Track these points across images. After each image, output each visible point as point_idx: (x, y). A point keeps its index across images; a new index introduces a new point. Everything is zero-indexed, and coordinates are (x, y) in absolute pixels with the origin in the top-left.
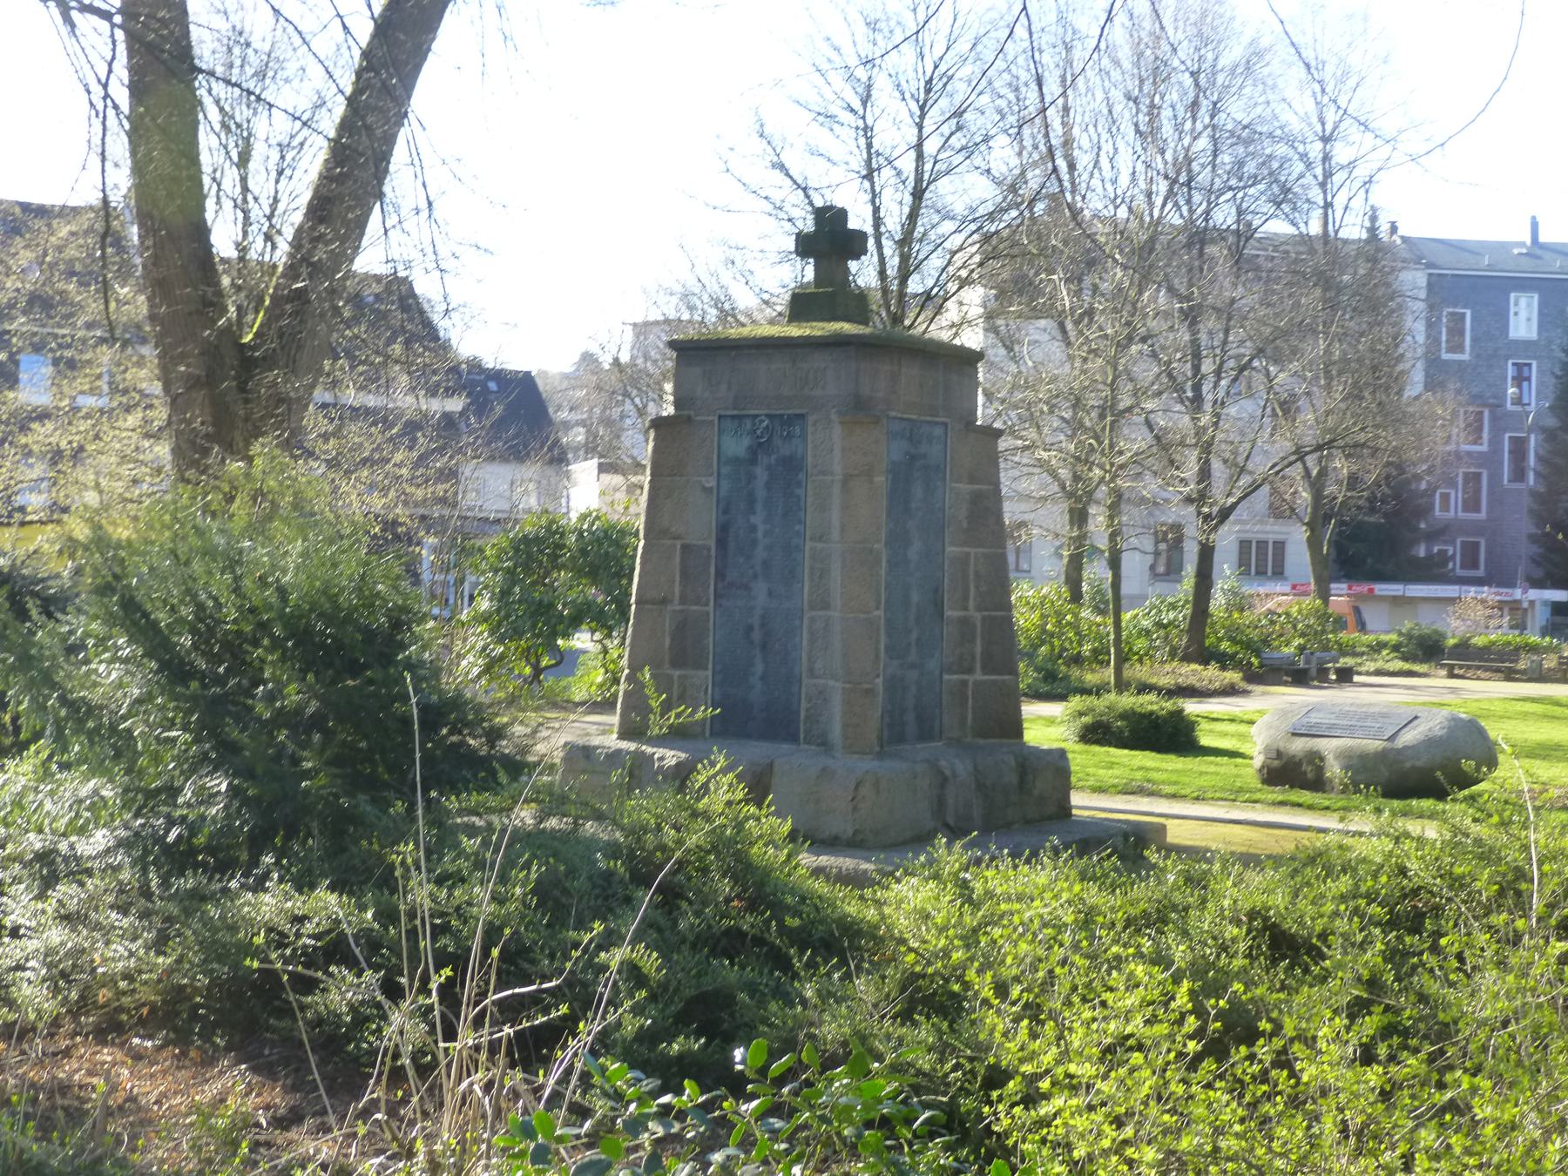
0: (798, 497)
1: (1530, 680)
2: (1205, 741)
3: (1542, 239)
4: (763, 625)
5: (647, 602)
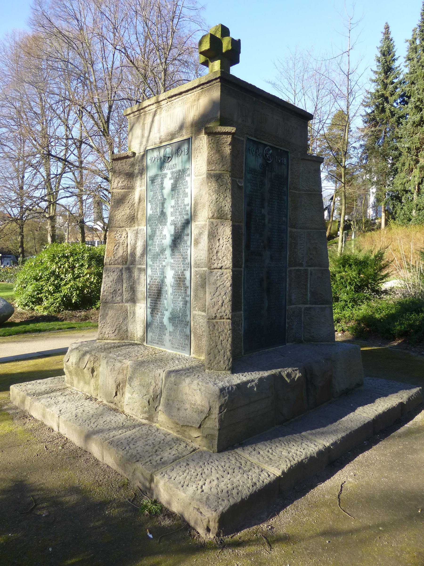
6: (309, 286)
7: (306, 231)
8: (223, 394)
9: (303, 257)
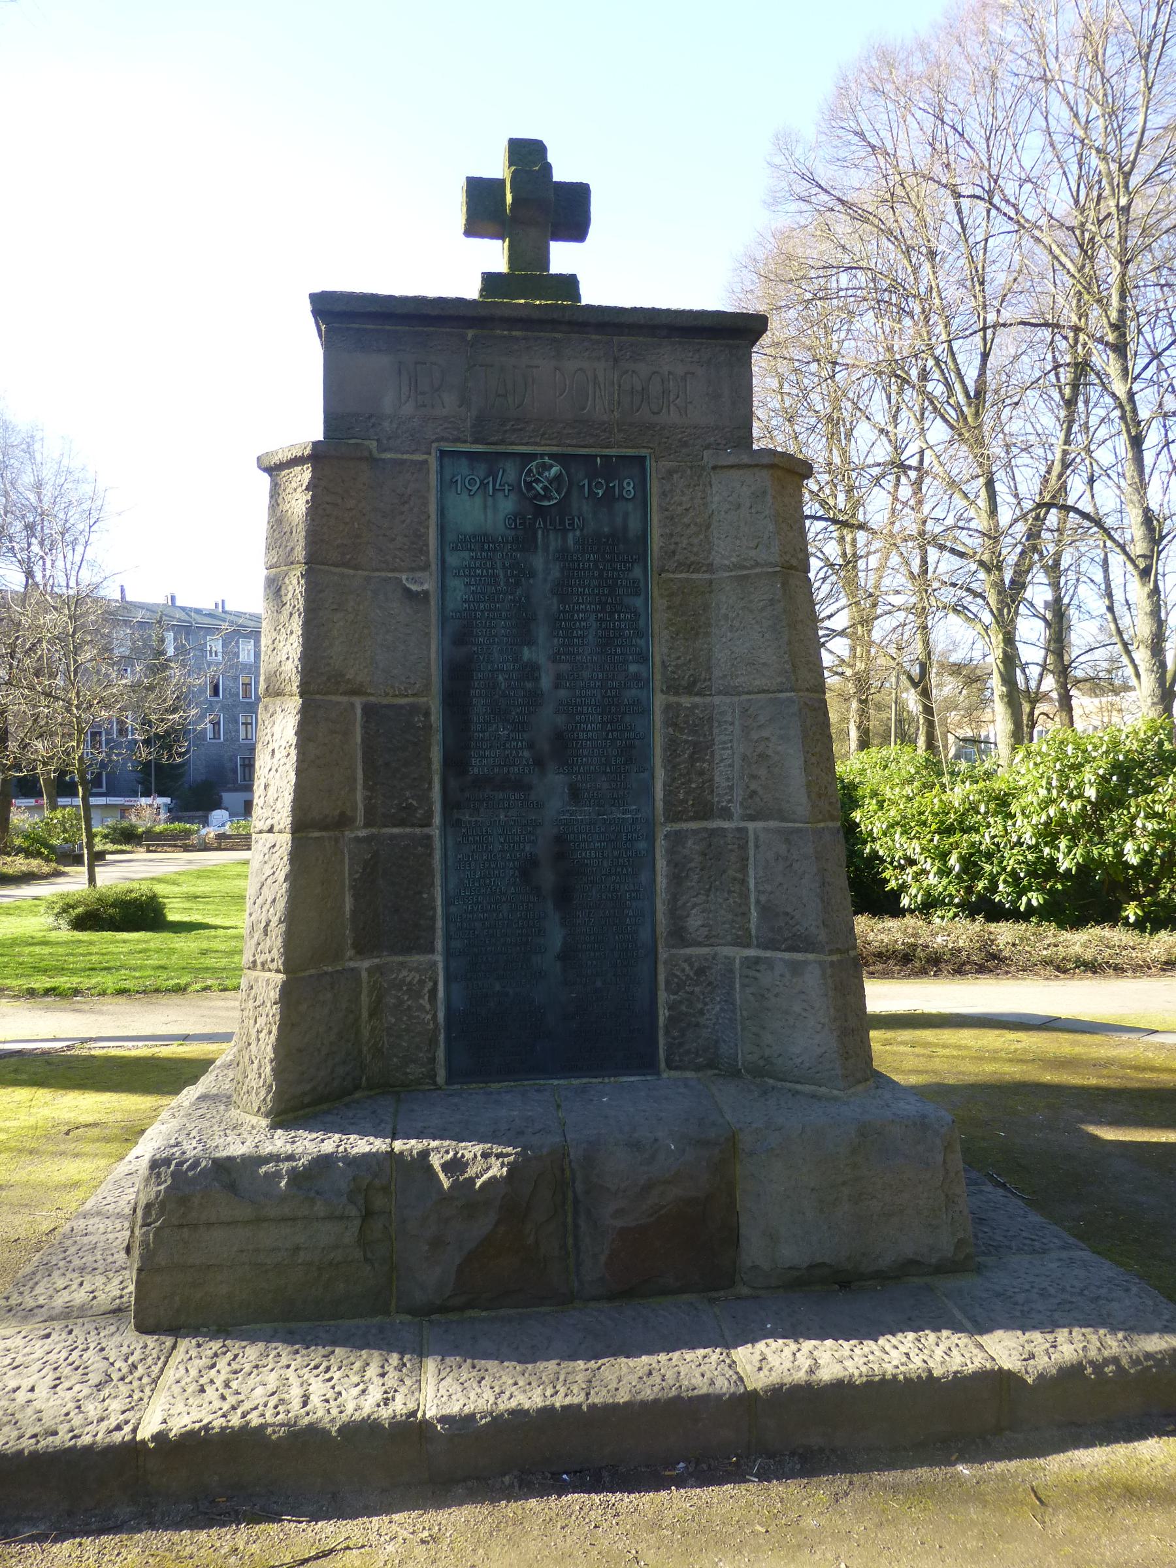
1: (199, 850)
2: (172, 917)
3: (128, 599)
6: (752, 886)
7: (736, 699)
8: (158, 1175)
9: (731, 788)
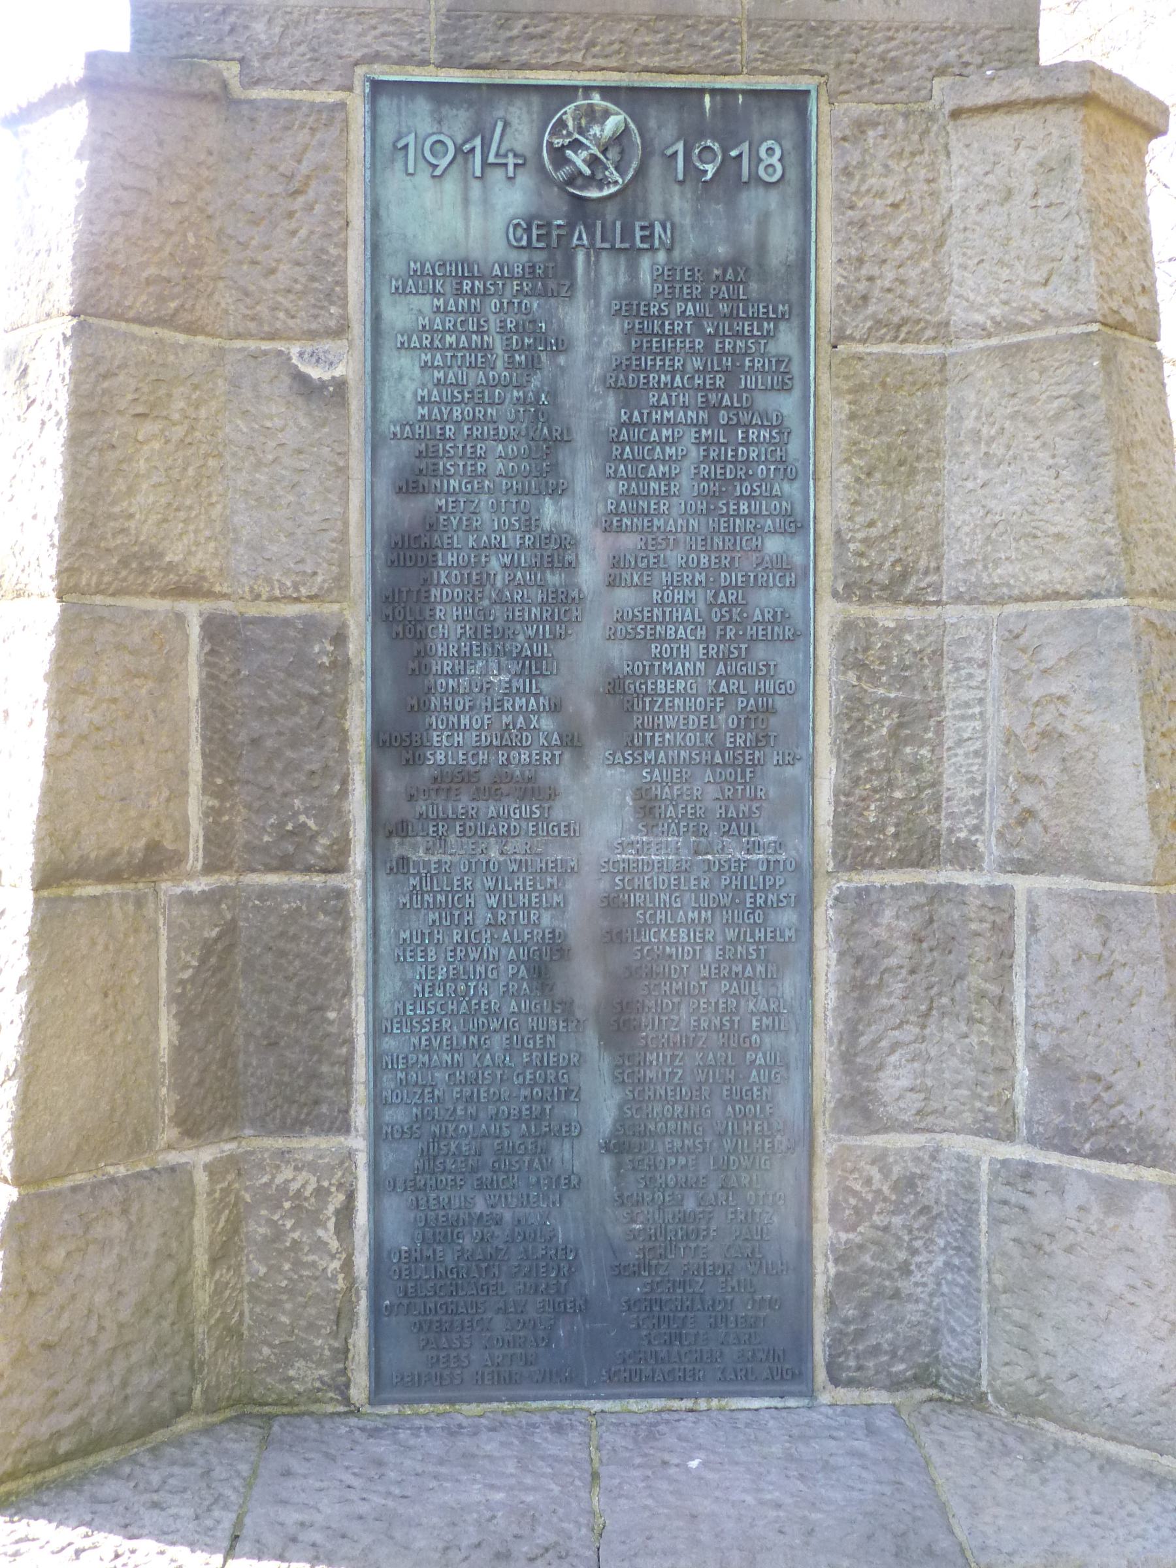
0: (781, 428)
4: (614, 938)
5: (83, 871)
7: (993, 612)
